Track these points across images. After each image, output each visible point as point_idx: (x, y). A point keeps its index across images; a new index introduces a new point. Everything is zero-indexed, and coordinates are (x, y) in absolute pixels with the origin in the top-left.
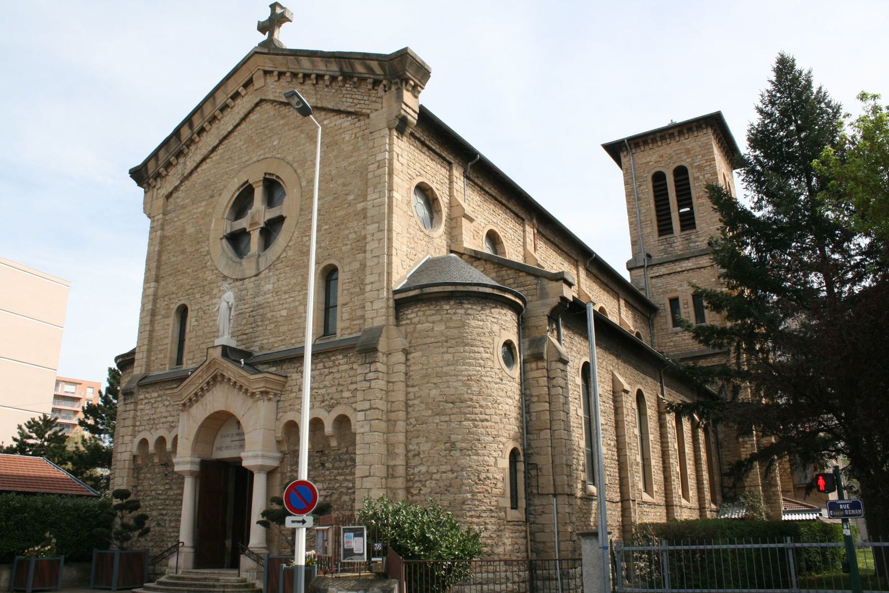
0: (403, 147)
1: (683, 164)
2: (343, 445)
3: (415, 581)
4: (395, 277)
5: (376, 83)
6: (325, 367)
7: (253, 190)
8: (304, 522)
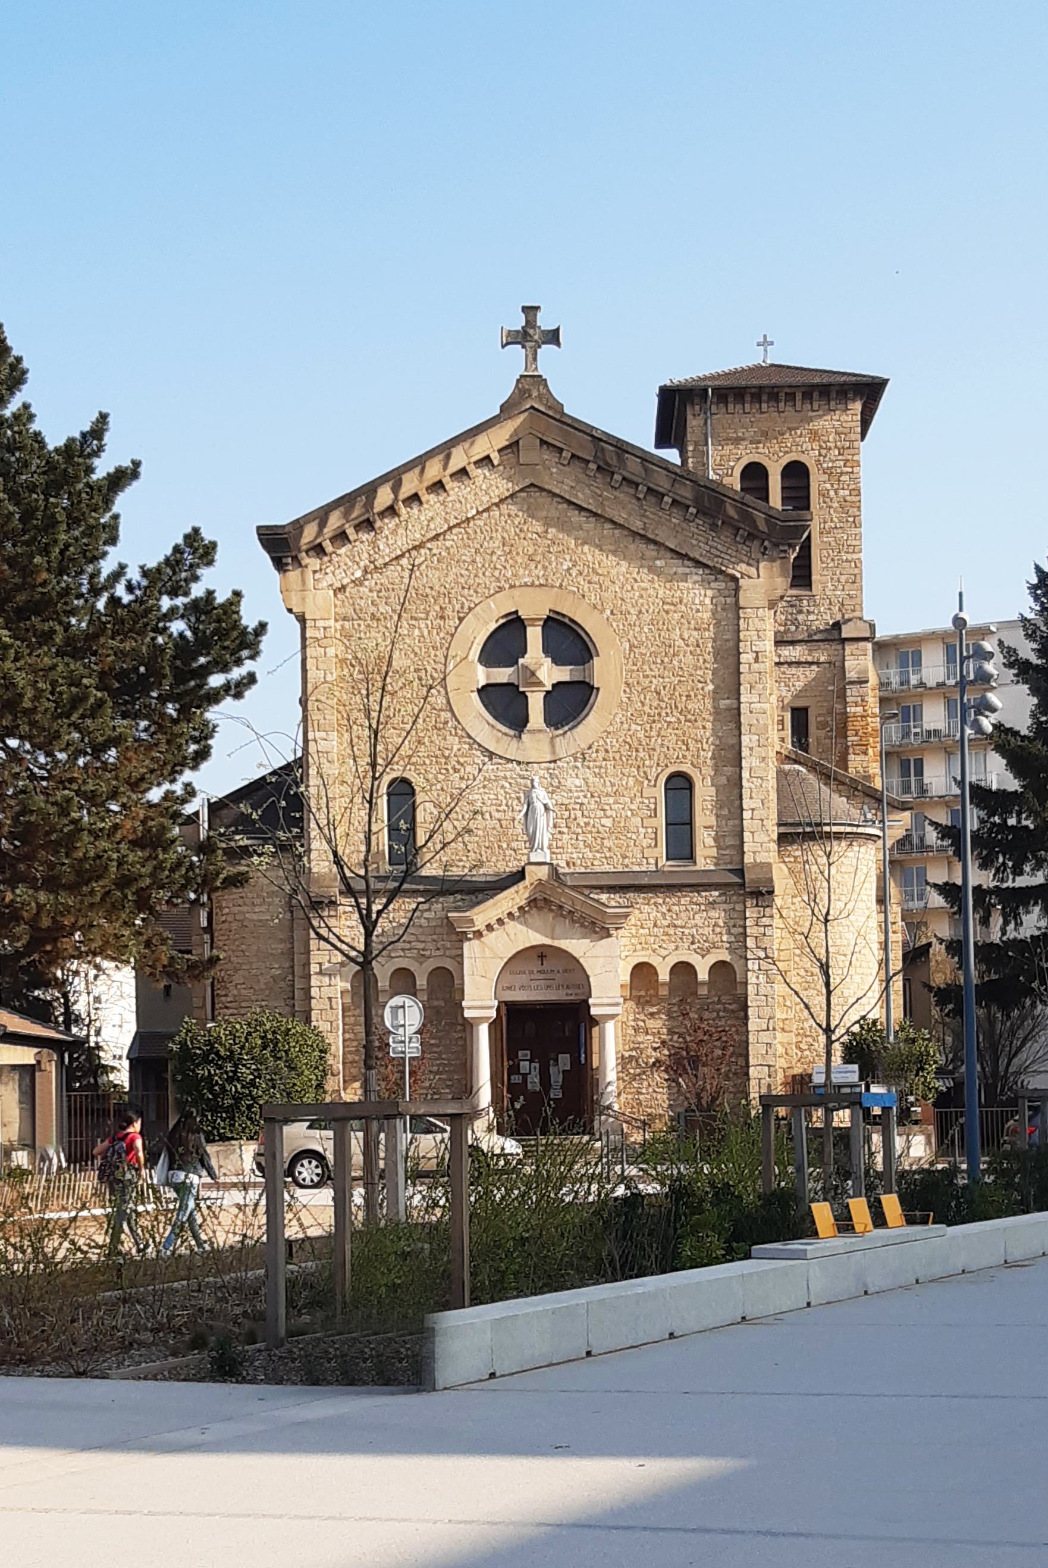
1: (803, 458)
2: (713, 993)
3: (59, 1190)
5: (751, 537)
6: (691, 902)
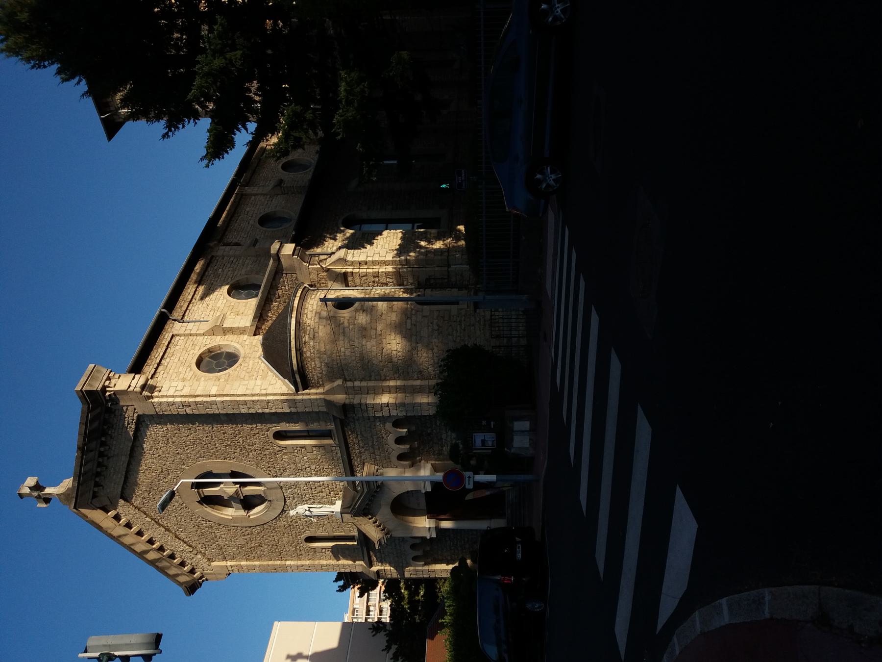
0: (168, 386)
4: (285, 390)
7: (206, 497)
8: (469, 477)
